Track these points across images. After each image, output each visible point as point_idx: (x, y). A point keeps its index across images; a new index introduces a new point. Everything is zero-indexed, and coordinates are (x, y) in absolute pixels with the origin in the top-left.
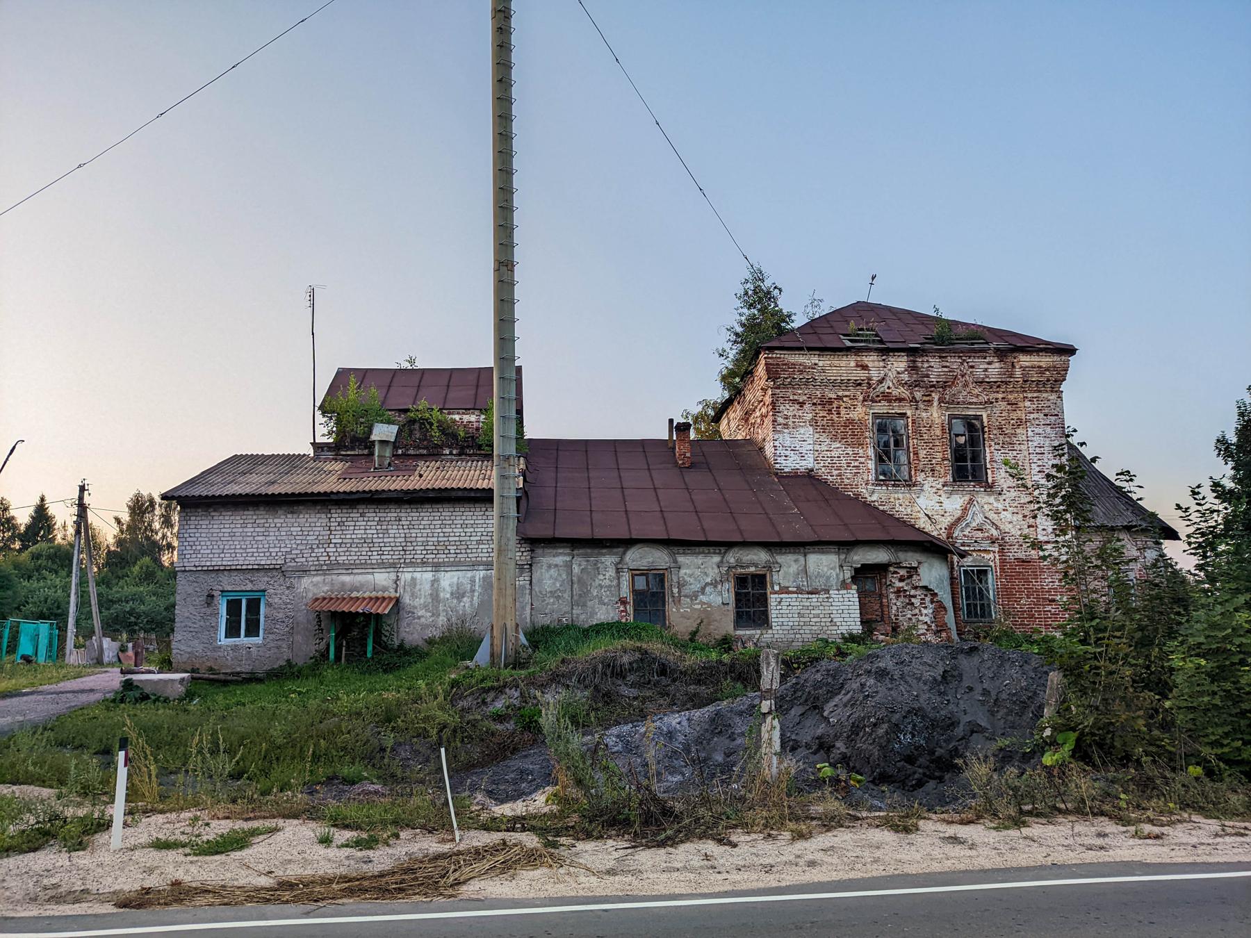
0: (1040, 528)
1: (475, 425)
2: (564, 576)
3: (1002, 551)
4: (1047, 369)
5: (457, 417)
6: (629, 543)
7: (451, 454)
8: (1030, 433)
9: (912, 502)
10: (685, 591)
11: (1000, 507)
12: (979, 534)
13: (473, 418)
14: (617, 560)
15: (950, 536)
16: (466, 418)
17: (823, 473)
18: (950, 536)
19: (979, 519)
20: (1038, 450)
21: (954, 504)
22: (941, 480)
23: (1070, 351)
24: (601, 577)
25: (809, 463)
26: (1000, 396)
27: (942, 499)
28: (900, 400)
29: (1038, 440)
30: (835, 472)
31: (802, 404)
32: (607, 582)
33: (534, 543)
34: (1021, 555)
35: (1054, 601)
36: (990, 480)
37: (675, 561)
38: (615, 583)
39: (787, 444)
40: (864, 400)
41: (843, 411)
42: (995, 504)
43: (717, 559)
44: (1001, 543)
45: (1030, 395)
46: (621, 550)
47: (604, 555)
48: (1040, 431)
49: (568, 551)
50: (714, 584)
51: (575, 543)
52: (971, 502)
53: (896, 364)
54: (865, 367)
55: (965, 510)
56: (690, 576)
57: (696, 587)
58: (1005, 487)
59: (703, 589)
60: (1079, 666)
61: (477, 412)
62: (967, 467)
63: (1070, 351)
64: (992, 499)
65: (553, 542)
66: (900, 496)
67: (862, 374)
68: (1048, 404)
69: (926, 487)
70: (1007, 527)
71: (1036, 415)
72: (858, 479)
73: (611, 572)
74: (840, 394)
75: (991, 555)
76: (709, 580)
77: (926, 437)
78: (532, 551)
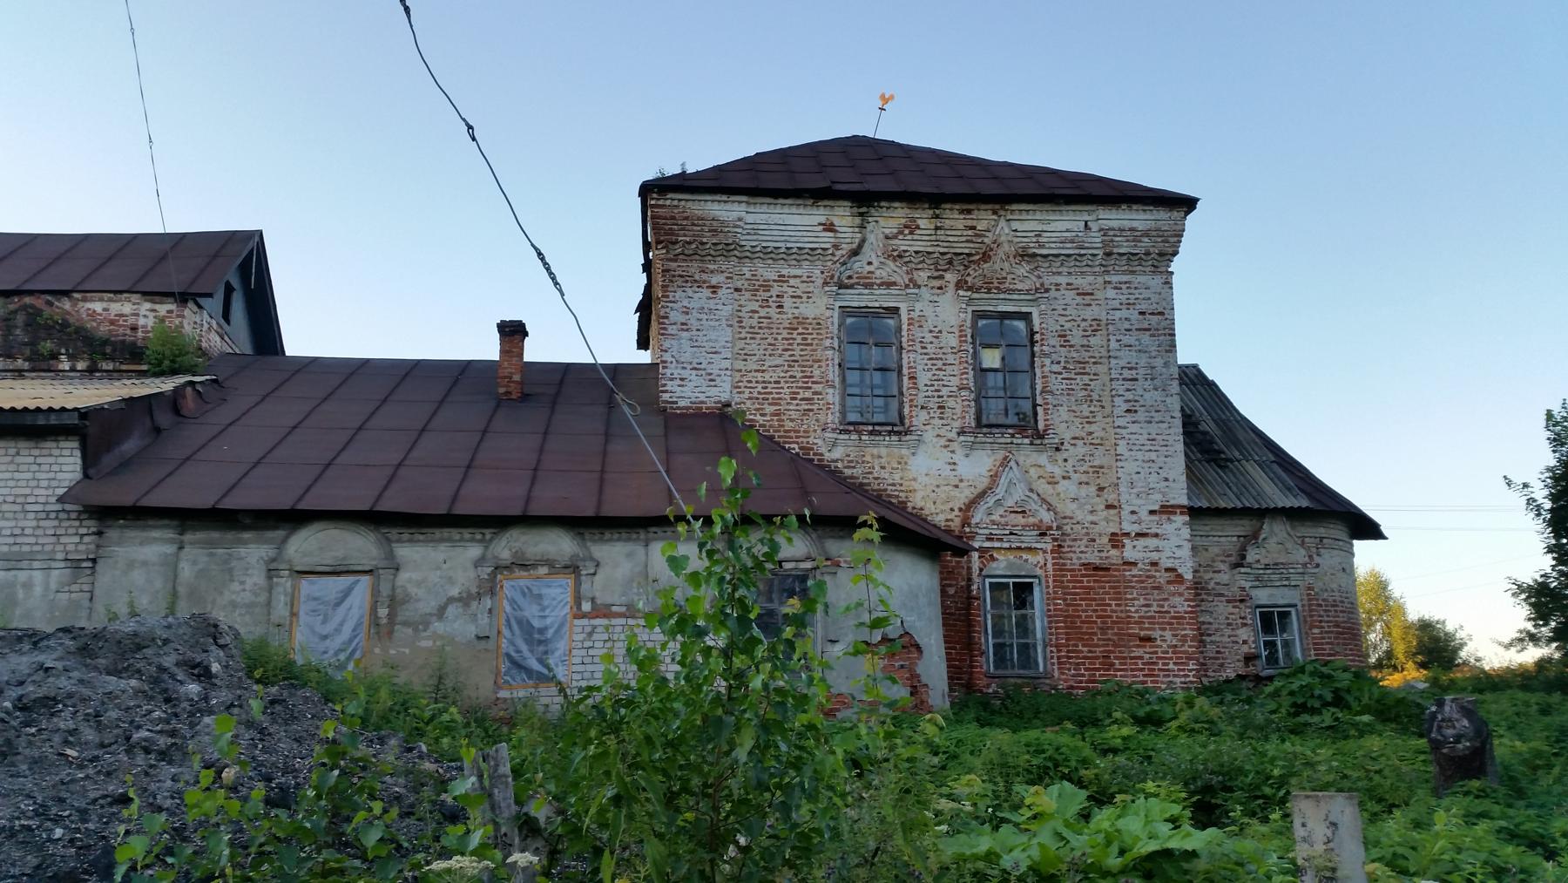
0: (1127, 509)
1: (131, 320)
2: (158, 584)
3: (1058, 549)
4: (1146, 234)
5: (98, 307)
6: (296, 518)
7: (73, 369)
8: (1113, 345)
9: (902, 463)
10: (404, 614)
11: (1058, 472)
12: (1019, 519)
13: (127, 308)
14: (272, 553)
15: (966, 522)
16: (116, 308)
17: (743, 402)
18: (966, 522)
19: (1019, 493)
20: (1127, 374)
21: (977, 466)
22: (957, 424)
23: (1189, 204)
24: (236, 586)
25: (722, 392)
26: (1063, 280)
27: (956, 458)
28: (889, 285)
29: (1127, 357)
30: (769, 409)
31: (714, 289)
32: (247, 597)
33: (105, 515)
34: (1093, 558)
35: (1149, 639)
36: (1041, 426)
37: (390, 556)
38: (262, 599)
39: (686, 357)
40: (826, 283)
41: (788, 302)
42: (1049, 468)
43: (475, 551)
44: (1056, 535)
45: (1115, 279)
46: (280, 533)
47: (245, 543)
48: (1132, 341)
49: (170, 534)
50: (465, 600)
51: (185, 518)
52: (1005, 462)
53: (882, 222)
54: (829, 227)
55: (994, 477)
56: (419, 584)
57: (428, 605)
58: (1067, 436)
59: (441, 612)
60: (804, 594)
61: (135, 298)
62: (1005, 414)
63: (1189, 204)
64: (1043, 459)
65: (139, 514)
66: (883, 451)
67: (826, 239)
68: (1146, 294)
69: (929, 435)
70: (1069, 508)
71: (1124, 313)
72: (811, 422)
73: (257, 578)
74: (784, 272)
75: (1040, 558)
76: (455, 592)
77: (931, 349)
78: (99, 533)
